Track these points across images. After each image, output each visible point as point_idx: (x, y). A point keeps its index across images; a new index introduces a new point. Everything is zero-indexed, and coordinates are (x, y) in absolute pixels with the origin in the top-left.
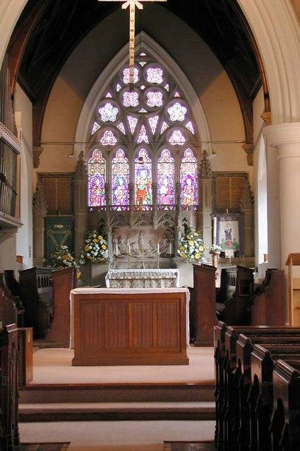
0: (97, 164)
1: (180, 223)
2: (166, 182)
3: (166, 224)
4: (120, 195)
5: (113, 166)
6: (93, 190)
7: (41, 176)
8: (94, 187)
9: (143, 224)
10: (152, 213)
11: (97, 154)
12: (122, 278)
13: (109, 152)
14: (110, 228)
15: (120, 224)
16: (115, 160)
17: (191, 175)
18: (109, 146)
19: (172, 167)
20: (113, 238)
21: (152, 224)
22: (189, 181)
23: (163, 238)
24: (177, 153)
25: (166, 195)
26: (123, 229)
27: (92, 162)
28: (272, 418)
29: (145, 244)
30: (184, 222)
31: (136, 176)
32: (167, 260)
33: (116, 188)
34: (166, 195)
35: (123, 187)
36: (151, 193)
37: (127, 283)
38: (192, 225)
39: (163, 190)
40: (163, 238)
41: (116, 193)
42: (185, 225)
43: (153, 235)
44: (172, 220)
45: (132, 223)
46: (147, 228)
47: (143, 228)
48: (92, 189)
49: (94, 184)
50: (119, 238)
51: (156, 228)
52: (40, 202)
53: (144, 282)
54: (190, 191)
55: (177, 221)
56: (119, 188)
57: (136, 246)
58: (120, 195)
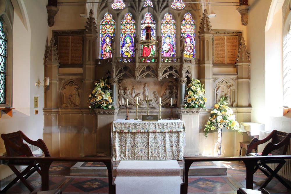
0: (108, 25)
1: (184, 75)
2: (168, 40)
3: (171, 75)
4: (127, 50)
5: (122, 27)
6: (104, 47)
7: (56, 34)
8: (105, 45)
9: (148, 76)
10: (134, 63)
11: (108, 17)
12: (126, 131)
13: (118, 14)
14: (116, 80)
15: (125, 76)
16: (124, 22)
17: (190, 35)
18: (118, 10)
19: (173, 27)
20: (119, 89)
21: (157, 75)
22: (188, 40)
23: (167, 89)
24: (178, 16)
25: (168, 51)
26: (128, 82)
27: (104, 23)
28: (277, 144)
29: (149, 94)
30: (187, 74)
31: (141, 35)
32: (169, 110)
33: (123, 46)
34: (168, 51)
35: (130, 44)
36: (154, 49)
37: (143, 133)
38: (193, 75)
39: (165, 47)
40: (167, 89)
41: (124, 49)
42: (187, 77)
43: (157, 87)
44: (176, 71)
45: (137, 73)
46: (151, 80)
47: (148, 79)
48: (102, 46)
49: (104, 42)
50: (125, 89)
51: (160, 79)
52: (51, 55)
53: (148, 136)
54: (189, 48)
55: (157, 70)
56: (127, 45)
57: (141, 97)
58: (127, 50)
